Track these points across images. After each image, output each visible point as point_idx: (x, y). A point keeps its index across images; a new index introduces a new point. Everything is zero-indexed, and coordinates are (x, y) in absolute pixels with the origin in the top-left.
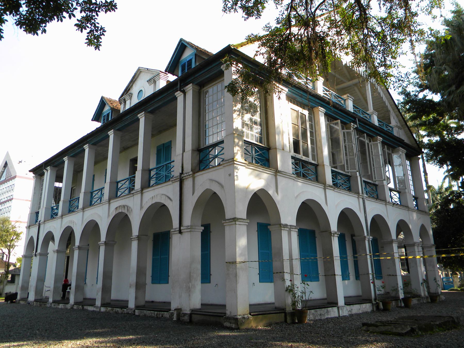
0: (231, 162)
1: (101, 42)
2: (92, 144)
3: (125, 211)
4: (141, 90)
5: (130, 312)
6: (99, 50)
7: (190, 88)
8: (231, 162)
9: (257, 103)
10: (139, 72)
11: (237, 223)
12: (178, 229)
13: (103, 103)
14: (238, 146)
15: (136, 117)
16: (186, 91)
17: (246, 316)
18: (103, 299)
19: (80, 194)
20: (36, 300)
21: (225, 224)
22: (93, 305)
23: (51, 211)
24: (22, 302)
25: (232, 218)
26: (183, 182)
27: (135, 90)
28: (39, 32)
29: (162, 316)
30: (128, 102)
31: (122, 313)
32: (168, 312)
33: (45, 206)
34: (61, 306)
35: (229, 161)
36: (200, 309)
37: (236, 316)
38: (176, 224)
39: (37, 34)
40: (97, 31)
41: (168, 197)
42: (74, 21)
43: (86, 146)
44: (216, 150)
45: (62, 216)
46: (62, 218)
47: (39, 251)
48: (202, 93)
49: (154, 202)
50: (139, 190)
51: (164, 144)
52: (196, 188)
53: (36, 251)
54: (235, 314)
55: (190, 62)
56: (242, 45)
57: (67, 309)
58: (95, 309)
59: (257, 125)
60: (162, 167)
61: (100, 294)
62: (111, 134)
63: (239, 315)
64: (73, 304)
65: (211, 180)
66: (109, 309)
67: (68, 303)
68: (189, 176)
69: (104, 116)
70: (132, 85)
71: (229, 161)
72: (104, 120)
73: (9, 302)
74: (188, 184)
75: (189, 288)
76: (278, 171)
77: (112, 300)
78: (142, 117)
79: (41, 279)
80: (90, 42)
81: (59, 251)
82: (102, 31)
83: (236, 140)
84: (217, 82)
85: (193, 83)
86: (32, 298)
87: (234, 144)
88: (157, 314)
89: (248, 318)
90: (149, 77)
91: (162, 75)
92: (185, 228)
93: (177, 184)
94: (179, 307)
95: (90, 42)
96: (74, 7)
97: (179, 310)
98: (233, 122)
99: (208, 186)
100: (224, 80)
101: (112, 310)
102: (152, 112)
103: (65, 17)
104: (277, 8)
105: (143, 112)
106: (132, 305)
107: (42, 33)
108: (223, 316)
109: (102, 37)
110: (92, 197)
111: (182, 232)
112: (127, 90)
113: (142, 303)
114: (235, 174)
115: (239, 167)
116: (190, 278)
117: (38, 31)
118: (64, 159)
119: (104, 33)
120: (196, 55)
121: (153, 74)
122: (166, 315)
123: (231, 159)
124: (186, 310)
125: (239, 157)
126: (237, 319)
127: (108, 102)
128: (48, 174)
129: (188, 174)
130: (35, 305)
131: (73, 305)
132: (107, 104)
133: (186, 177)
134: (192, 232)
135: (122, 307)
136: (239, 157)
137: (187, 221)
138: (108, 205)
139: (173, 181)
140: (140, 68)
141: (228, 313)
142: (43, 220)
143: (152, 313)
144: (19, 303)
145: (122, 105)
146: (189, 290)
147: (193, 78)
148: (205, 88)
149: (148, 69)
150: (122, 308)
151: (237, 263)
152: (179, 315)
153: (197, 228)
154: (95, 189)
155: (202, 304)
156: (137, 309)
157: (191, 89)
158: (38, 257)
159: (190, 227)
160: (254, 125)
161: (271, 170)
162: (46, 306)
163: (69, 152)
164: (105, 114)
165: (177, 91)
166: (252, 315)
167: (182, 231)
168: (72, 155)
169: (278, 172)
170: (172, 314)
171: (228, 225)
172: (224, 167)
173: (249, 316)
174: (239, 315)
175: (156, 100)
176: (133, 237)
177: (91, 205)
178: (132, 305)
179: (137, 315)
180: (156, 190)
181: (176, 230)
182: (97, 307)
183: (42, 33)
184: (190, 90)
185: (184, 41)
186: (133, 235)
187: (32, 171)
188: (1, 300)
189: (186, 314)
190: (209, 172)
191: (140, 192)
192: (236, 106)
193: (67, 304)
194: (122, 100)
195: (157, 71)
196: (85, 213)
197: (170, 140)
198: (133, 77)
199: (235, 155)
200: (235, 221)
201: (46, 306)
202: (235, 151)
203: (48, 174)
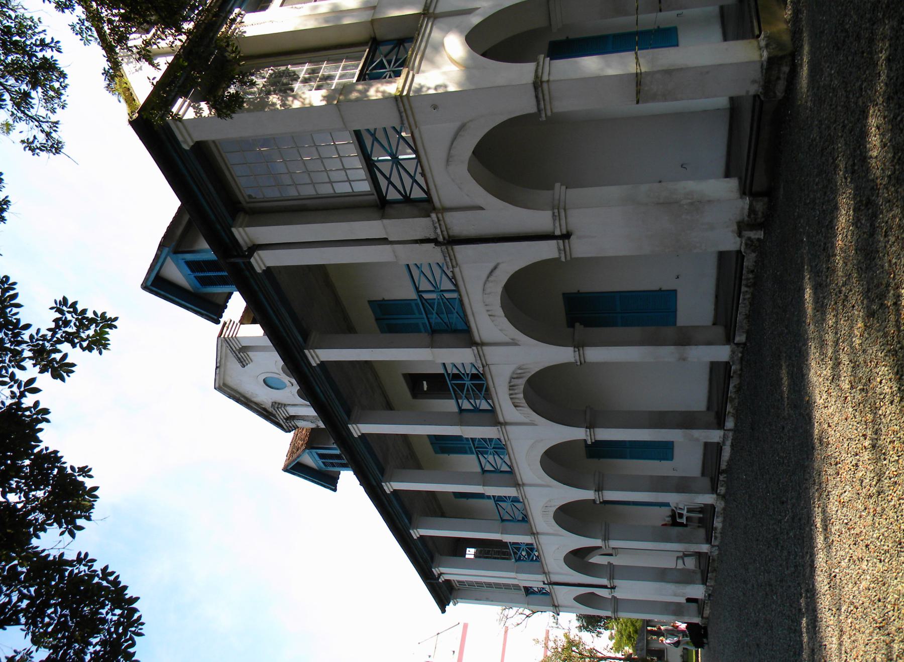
0: (404, 106)
1: (95, 313)
2: (382, 476)
3: (522, 382)
4: (265, 381)
5: (740, 355)
6: (116, 319)
7: (245, 234)
8: (404, 106)
9: (268, 72)
10: (224, 387)
11: (545, 78)
12: (561, 242)
13: (295, 468)
14: (367, 90)
15: (318, 369)
16: (250, 245)
17: (763, 43)
18: (708, 427)
20: (704, 582)
21: (549, 113)
22: (719, 447)
23: (523, 562)
24: (707, 612)
25: (533, 94)
26: (453, 236)
27: (265, 396)
28: (89, 483)
29: (752, 271)
30: (292, 411)
31: (740, 376)
32: (743, 256)
33: (513, 575)
34: (718, 523)
35: (402, 110)
36: (740, 179)
37: (762, 65)
38: (547, 250)
39: (96, 488)
40: (67, 323)
41: (488, 277)
42: (45, 380)
43: (385, 488)
44: (380, 158)
45: (533, 534)
46: (538, 533)
47: (604, 582)
48: (252, 205)
49: (500, 312)
50: (476, 351)
51: (377, 319)
52: (467, 201)
53: (605, 587)
54: (758, 67)
55: (194, 266)
56: (130, 98)
57: (724, 509)
58: (729, 443)
59: (321, 68)
60: (424, 301)
61: (696, 433)
62: (359, 429)
63: (761, 56)
64: (715, 496)
65: (448, 161)
66: (729, 408)
67: (713, 507)
68: (442, 223)
69: (325, 465)
70: (256, 404)
71: (402, 110)
72: (333, 465)
73: (705, 640)
74: (459, 224)
75: (692, 204)
76: (424, 10)
77: (709, 408)
78: (317, 356)
79: (661, 575)
80: (99, 343)
81: (605, 535)
82: (65, 308)
83: (354, 95)
84: (224, 167)
85: (231, 227)
86: (698, 591)
87: (363, 100)
88: (747, 286)
89: (769, 38)
90: (233, 365)
91: (226, 333)
92: (557, 224)
94: (735, 227)
95: (99, 343)
96: (9, 381)
97: (741, 227)
98: (312, 107)
99: (461, 169)
100: (214, 142)
101: (732, 400)
102: (306, 336)
103: (37, 404)
104: (44, 31)
105: (306, 351)
106: (722, 353)
107: (91, 477)
108: (762, 102)
109: (80, 308)
111: (568, 232)
112: (267, 414)
113: (720, 331)
114: (432, 92)
115: (415, 85)
116: (669, 205)
117: (86, 487)
118: (415, 538)
119: (70, 303)
120: (176, 252)
121: (226, 356)
122: (749, 261)
123: (397, 105)
124: (743, 208)
125: (392, 88)
126: (771, 61)
127: (295, 456)
128: (450, 572)
129: (437, 225)
130: (712, 583)
131: (718, 495)
132: (298, 457)
133: (444, 228)
134: (567, 207)
135: (728, 377)
136: (392, 88)
137: (541, 220)
138: (508, 428)
139: (454, 263)
140: (217, 385)
141: (754, 89)
142: (542, 577)
143: (744, 299)
144: (707, 618)
145: (300, 424)
146: (698, 204)
147: (219, 227)
148: (241, 199)
149: (217, 367)
150: (730, 377)
151: (639, 71)
152: (752, 226)
153: (557, 197)
155: (727, 175)
156: (734, 339)
157: (245, 231)
158: (617, 582)
159: (556, 211)
160: (320, 75)
161: (422, 26)
162: (716, 558)
163: (400, 526)
164: (320, 462)
165: (250, 263)
166: (760, 33)
167: (564, 232)
168: (406, 521)
169: (428, 10)
170: (750, 243)
171: (550, 103)
172: (416, 127)
173: (762, 36)
174: (761, 56)
175: (277, 322)
176: (577, 358)
177: (525, 519)
178: (722, 353)
179: (747, 338)
180: (474, 310)
181: (562, 247)
182: (725, 437)
183: (91, 477)
184: (246, 233)
185: (146, 279)
186: (573, 360)
187: (443, 606)
188: (699, 657)
189: (751, 205)
190: (431, 171)
191: (479, 347)
192: (274, 104)
193: (715, 508)
194: (285, 423)
195: (219, 345)
196: (525, 481)
197: (367, 304)
198: (238, 400)
199: (386, 95)
200: (542, 82)
201: (716, 558)
202: (380, 96)
203: (450, 572)
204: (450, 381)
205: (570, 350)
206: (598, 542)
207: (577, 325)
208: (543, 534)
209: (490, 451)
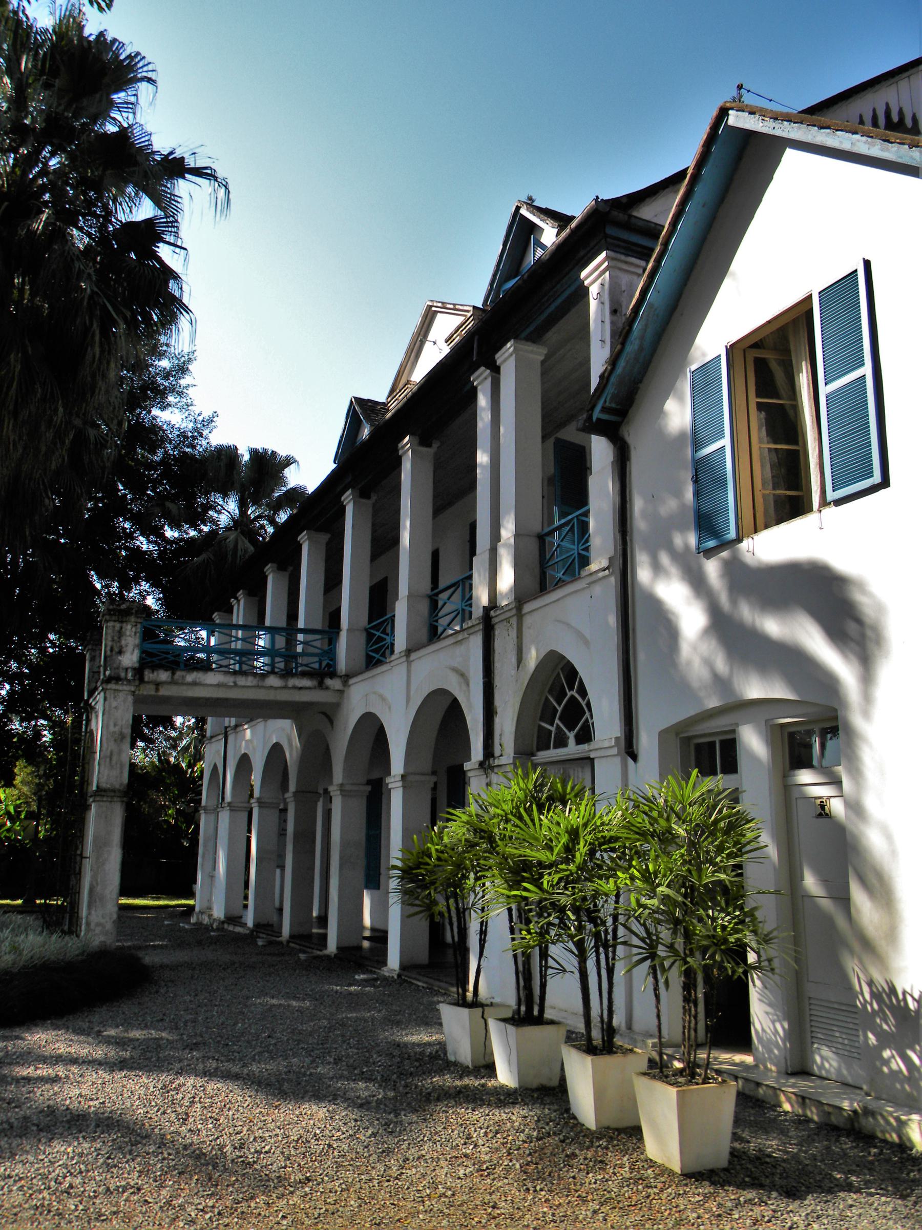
19: (397, 604)
43: (267, 567)
45: (408, 652)
93: (476, 643)
102: (535, 338)
110: (434, 606)
154: (442, 585)
177: (434, 635)
190: (576, 592)
191: (514, 612)
196: (414, 666)
204: (577, 516)
205: (401, 771)
206: (292, 787)
207: (369, 788)
208: (265, 727)
209: (575, 547)
